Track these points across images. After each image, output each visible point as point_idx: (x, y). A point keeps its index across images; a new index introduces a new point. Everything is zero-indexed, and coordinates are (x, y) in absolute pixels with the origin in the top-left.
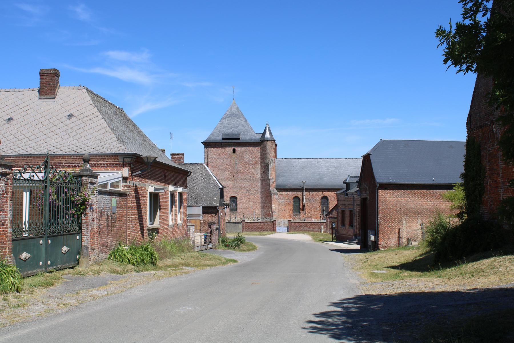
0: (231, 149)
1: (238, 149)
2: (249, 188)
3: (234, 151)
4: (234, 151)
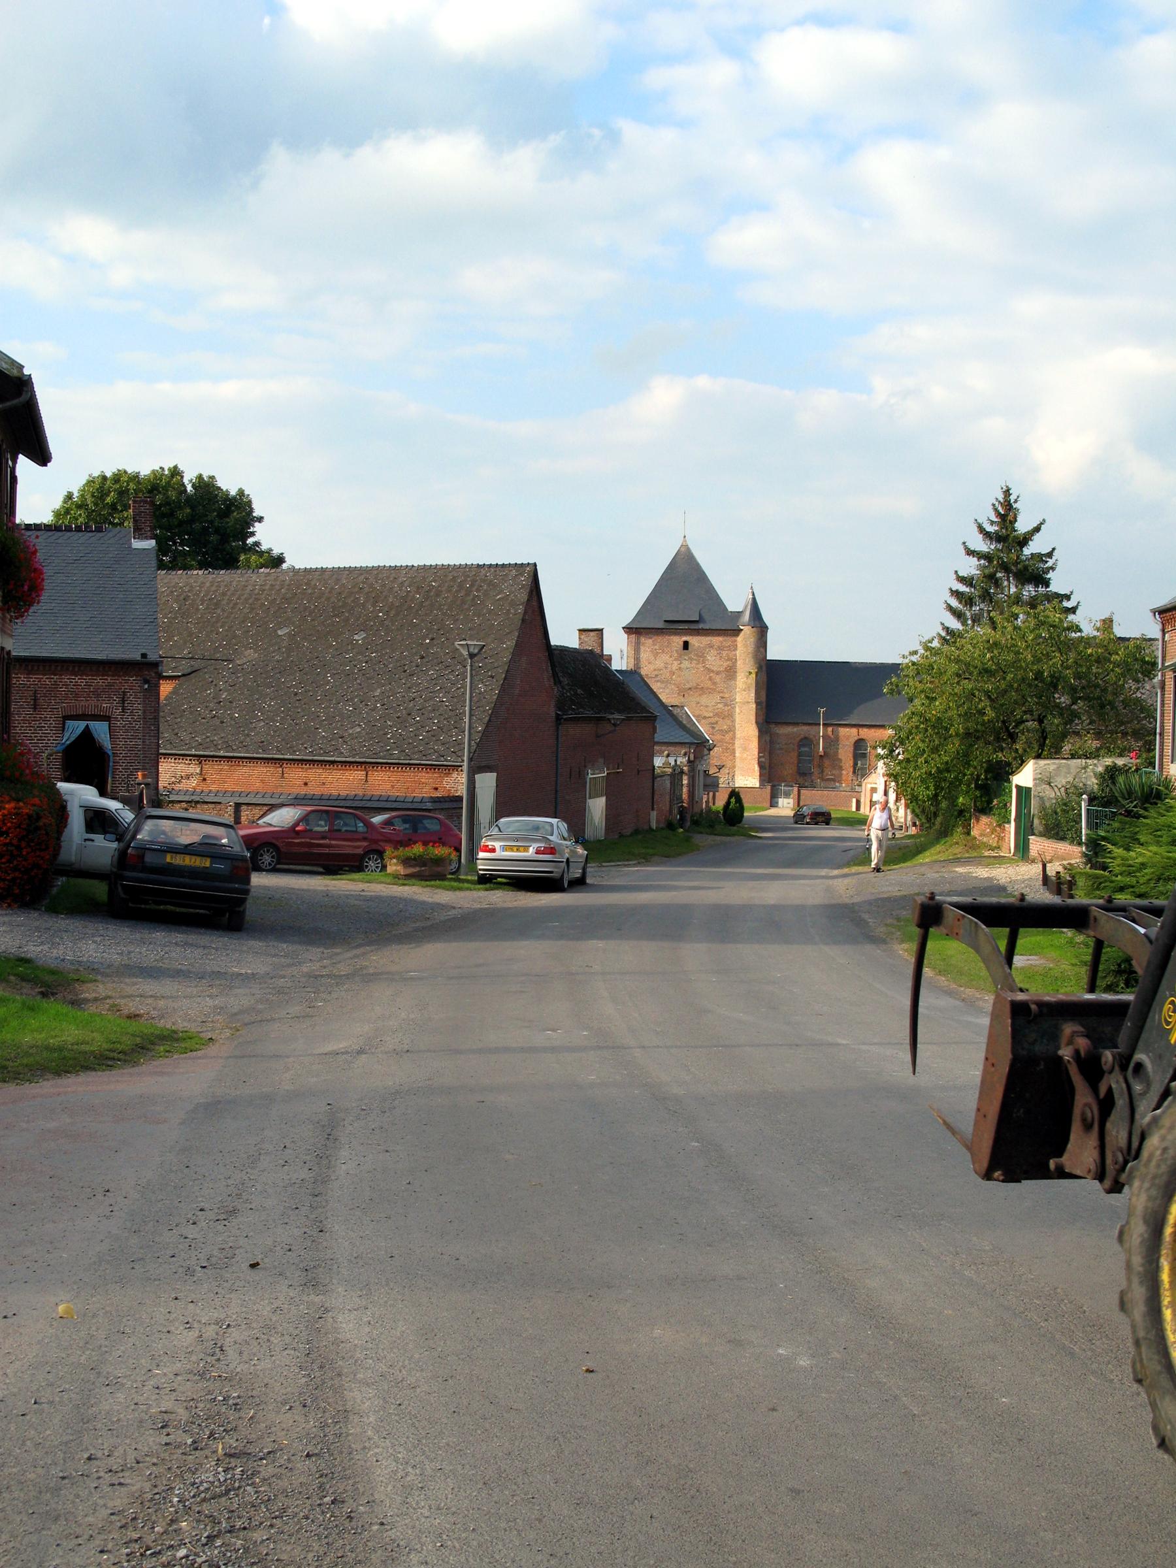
0: (678, 641)
1: (694, 641)
2: (713, 720)
3: (686, 645)
4: (686, 645)
